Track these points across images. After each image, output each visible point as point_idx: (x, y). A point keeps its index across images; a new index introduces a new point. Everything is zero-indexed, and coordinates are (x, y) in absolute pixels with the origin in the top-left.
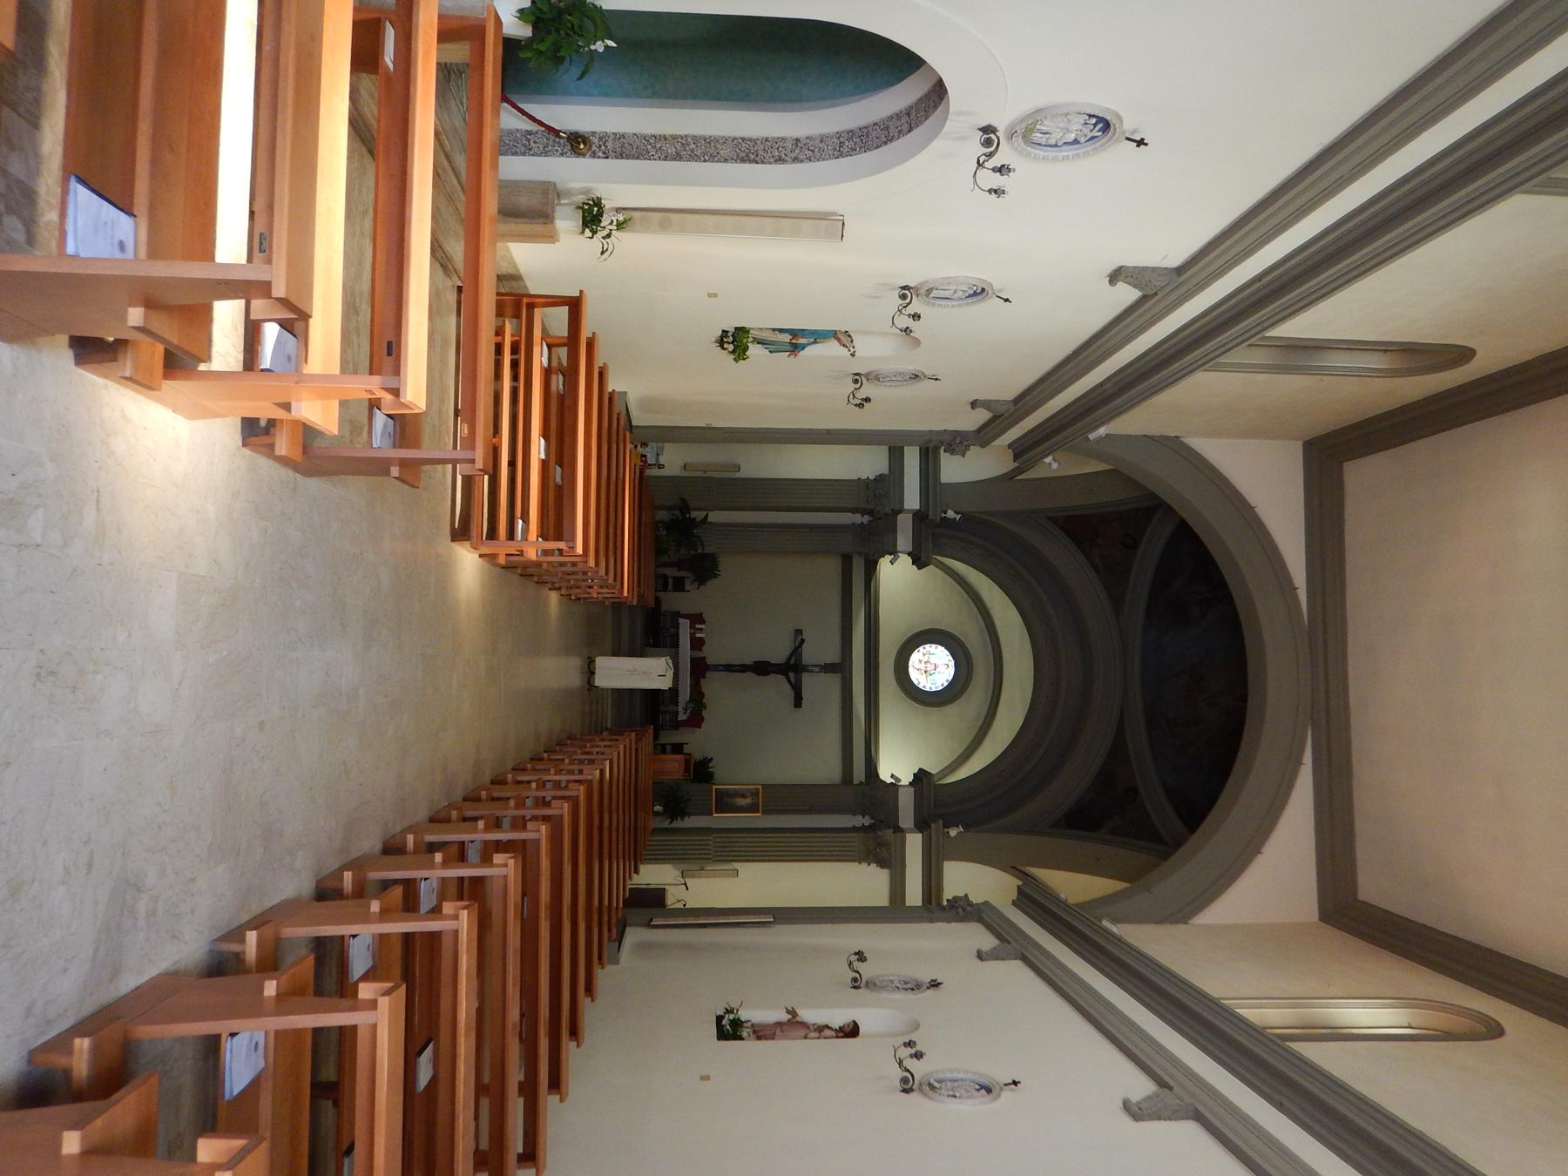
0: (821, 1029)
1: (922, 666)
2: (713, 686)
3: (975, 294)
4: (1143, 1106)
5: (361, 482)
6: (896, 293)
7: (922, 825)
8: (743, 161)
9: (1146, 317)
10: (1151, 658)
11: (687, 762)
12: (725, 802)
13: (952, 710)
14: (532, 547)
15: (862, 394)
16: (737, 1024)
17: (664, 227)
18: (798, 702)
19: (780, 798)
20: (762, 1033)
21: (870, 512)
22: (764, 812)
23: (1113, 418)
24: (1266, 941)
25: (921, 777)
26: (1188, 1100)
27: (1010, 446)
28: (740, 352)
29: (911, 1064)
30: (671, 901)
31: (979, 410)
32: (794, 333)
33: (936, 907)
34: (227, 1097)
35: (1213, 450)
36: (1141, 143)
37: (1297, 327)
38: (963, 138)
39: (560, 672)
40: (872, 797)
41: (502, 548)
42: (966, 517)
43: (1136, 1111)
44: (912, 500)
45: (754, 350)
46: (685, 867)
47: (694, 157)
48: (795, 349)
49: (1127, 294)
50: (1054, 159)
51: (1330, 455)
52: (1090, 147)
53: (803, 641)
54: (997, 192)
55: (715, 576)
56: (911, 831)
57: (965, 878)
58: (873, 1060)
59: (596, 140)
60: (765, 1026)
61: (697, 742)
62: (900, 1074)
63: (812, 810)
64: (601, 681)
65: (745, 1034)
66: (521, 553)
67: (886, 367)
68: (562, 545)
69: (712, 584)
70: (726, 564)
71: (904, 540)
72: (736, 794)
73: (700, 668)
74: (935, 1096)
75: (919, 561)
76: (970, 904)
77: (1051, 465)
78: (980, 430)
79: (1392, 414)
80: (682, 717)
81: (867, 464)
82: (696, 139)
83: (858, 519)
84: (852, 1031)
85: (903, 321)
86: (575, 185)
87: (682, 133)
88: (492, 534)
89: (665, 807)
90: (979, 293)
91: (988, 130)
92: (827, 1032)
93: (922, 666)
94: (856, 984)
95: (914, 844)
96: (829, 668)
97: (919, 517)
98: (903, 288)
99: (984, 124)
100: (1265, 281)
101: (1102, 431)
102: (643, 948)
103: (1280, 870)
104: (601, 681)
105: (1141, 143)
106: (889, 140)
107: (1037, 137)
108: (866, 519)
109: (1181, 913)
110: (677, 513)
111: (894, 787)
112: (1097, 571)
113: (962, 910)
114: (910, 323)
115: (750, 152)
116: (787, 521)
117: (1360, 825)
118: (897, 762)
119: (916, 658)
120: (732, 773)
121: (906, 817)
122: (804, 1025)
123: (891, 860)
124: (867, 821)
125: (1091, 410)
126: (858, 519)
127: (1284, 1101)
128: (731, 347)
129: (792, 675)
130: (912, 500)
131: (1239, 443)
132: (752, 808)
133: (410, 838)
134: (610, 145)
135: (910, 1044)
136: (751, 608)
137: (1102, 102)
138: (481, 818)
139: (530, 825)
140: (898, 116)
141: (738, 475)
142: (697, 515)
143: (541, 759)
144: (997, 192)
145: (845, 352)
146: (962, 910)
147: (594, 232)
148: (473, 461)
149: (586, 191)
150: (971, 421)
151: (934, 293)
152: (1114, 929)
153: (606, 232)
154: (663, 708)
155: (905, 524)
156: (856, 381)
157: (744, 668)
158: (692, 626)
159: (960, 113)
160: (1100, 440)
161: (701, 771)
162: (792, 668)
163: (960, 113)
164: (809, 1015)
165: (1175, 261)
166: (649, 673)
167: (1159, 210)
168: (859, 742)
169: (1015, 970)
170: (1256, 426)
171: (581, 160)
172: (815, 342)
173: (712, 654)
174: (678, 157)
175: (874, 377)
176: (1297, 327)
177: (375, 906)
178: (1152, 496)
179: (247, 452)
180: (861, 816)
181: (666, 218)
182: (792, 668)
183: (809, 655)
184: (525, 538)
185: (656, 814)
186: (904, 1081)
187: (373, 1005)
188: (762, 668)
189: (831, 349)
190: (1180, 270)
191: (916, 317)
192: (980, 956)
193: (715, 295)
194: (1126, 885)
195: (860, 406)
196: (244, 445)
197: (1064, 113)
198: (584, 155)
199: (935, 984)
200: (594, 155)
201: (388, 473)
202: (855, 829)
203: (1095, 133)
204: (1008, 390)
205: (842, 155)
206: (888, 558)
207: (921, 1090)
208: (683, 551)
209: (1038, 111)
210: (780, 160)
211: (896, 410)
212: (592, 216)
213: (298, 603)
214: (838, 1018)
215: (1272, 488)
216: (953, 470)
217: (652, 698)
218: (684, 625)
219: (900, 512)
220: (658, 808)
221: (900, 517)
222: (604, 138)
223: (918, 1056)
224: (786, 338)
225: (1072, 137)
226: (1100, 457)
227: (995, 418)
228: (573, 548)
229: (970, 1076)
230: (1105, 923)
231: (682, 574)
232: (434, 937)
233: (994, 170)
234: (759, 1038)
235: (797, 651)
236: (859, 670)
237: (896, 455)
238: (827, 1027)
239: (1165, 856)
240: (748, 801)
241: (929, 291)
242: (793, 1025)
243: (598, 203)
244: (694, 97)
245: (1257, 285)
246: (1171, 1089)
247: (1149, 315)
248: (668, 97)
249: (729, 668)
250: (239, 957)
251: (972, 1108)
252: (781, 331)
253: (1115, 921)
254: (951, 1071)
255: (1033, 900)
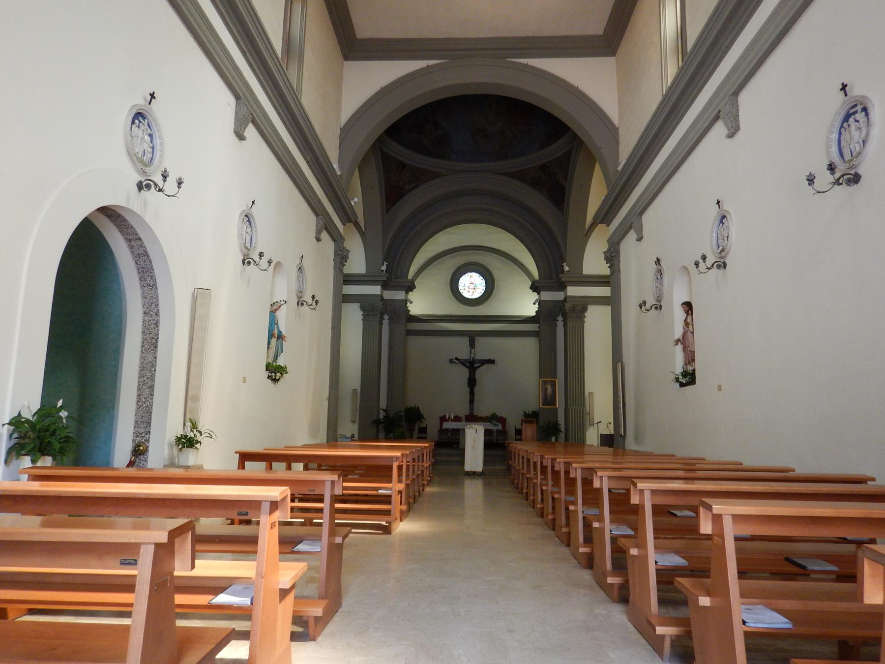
0: (686, 324)
1: (471, 291)
2: (483, 410)
3: (249, 221)
4: (730, 125)
5: (346, 579)
6: (246, 267)
7: (562, 287)
8: (156, 347)
9: (266, 123)
10: (467, 156)
11: (526, 422)
12: (550, 401)
13: (496, 274)
14: (394, 487)
15: (310, 301)
16: (685, 374)
17: (196, 399)
18: (491, 362)
19: (547, 368)
20: (690, 358)
21: (382, 314)
22: (555, 377)
23: (330, 162)
24: (626, 87)
25: (535, 288)
26: (727, 99)
27: (344, 225)
28: (282, 370)
29: (710, 260)
30: (611, 430)
31: (246, 134)
32: (271, 336)
33: (611, 280)
34: (789, 626)
35: (347, 112)
36: (152, 96)
37: (277, 44)
38: (145, 203)
39: (473, 490)
40: (548, 314)
41: (396, 506)
42: (385, 259)
43: (734, 131)
44: (376, 290)
45: (281, 362)
46: (587, 424)
47: (152, 378)
48: (280, 337)
49: (251, 132)
50: (162, 151)
51: (352, 46)
52: (155, 128)
53: (456, 359)
54: (180, 183)
55: (418, 408)
56: (566, 293)
57: (593, 262)
58: (707, 289)
59: (138, 440)
60: (686, 357)
61: (514, 421)
62: (715, 269)
63: (554, 349)
64: (479, 468)
65: (691, 368)
66: (400, 492)
67: (294, 286)
68: (395, 465)
69: (423, 411)
70: (411, 404)
71: (399, 295)
72: (545, 394)
73: (472, 418)
74: (728, 248)
75: (410, 287)
76: (609, 249)
77: (356, 201)
78: (334, 240)
79: (334, 23)
80: (500, 427)
81: (353, 316)
82: (141, 376)
83: (386, 322)
84: (688, 307)
85: (264, 263)
86: (166, 452)
87: (136, 385)
88: (387, 513)
89: (553, 435)
90: (248, 218)
91: (140, 186)
92: (689, 320)
93: (471, 291)
94: (659, 308)
95: (573, 291)
96: (472, 344)
97: (385, 286)
98: (244, 263)
99: (136, 188)
100: (245, 50)
101: (335, 166)
102: (638, 439)
103: (590, 79)
104: (479, 468)
105: (152, 96)
106: (146, 254)
107: (146, 159)
108: (386, 317)
109: (612, 131)
110: (381, 426)
111: (541, 303)
112: (416, 187)
113: (612, 257)
114: (265, 259)
115: (151, 343)
116: (386, 373)
117: (562, 33)
118: (525, 304)
119: (467, 294)
120: (533, 401)
121: (558, 296)
122: (684, 334)
123: (583, 304)
124: (560, 318)
125: (325, 174)
126: (386, 322)
127: (726, 44)
128: (278, 375)
129: (476, 365)
130: (376, 290)
131: (345, 95)
132: (553, 384)
133: (581, 550)
134: (142, 430)
135: (697, 264)
136: (438, 390)
137: (124, 116)
138: (567, 509)
139: (572, 475)
140: (131, 247)
141: (359, 391)
142: (382, 415)
143: (527, 493)
144: (180, 183)
145: (284, 308)
146: (612, 257)
147: (198, 442)
148: (333, 482)
149: (171, 446)
150: (328, 244)
151: (248, 245)
152: (623, 160)
153: (198, 434)
154: (495, 440)
155: (389, 295)
156: (302, 304)
157: (472, 393)
158: (447, 421)
159: (128, 201)
160: (340, 167)
161: (531, 417)
162: (472, 365)
163: (128, 201)
164: (678, 333)
165: (232, 100)
166: (474, 439)
167: (200, 109)
168: (513, 327)
169: (650, 219)
170: (335, 85)
171: (150, 449)
172: (277, 324)
173: (464, 411)
174: (152, 387)
175: (300, 294)
176: (277, 44)
177: (634, 552)
178: (374, 146)
179: (319, 639)
180: (557, 323)
181: (191, 398)
182: (472, 365)
183: (464, 355)
184: (391, 489)
185: (557, 440)
186: (719, 267)
187: (717, 519)
188: (472, 382)
189: (281, 315)
190: (237, 98)
191: (261, 255)
192: (640, 239)
193: (244, 378)
194: (597, 165)
195: (317, 302)
196: (314, 640)
197: (130, 138)
198: (147, 447)
199: (658, 262)
200: (148, 440)
201: (340, 546)
202: (565, 325)
203: (146, 123)
204: (311, 219)
205: (155, 285)
206: (408, 304)
207: (723, 257)
208: (403, 424)
209: (129, 153)
210: (157, 324)
211: (321, 282)
212: (187, 442)
213: (427, 611)
214: (679, 314)
215: (370, 79)
216: (357, 264)
217: (488, 445)
218: (447, 425)
219: (382, 296)
220: (553, 439)
221: (385, 297)
222: (137, 434)
223: (704, 258)
224: (274, 341)
225: (147, 138)
226: (351, 174)
227: (326, 229)
228: (397, 458)
229: (715, 230)
230: (619, 169)
231: (417, 428)
232: (658, 510)
233: (165, 181)
234: (693, 360)
235: (462, 362)
236: (475, 325)
237: (348, 299)
238: (685, 320)
239: (581, 142)
240: (549, 387)
241: (246, 248)
242: (685, 341)
243: (179, 440)
244: (116, 382)
245: (247, 53)
246: (720, 111)
247: (266, 123)
248: (114, 398)
249: (472, 401)
250: (676, 641)
251: (734, 226)
252: (269, 343)
253: (618, 164)
254: (712, 242)
255: (606, 215)
